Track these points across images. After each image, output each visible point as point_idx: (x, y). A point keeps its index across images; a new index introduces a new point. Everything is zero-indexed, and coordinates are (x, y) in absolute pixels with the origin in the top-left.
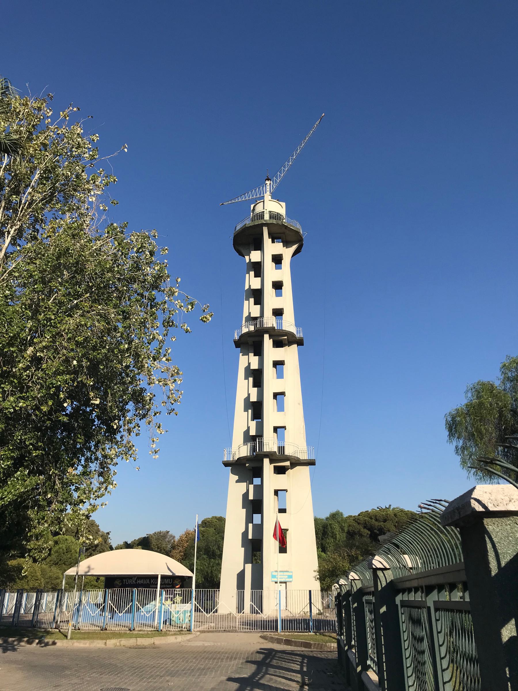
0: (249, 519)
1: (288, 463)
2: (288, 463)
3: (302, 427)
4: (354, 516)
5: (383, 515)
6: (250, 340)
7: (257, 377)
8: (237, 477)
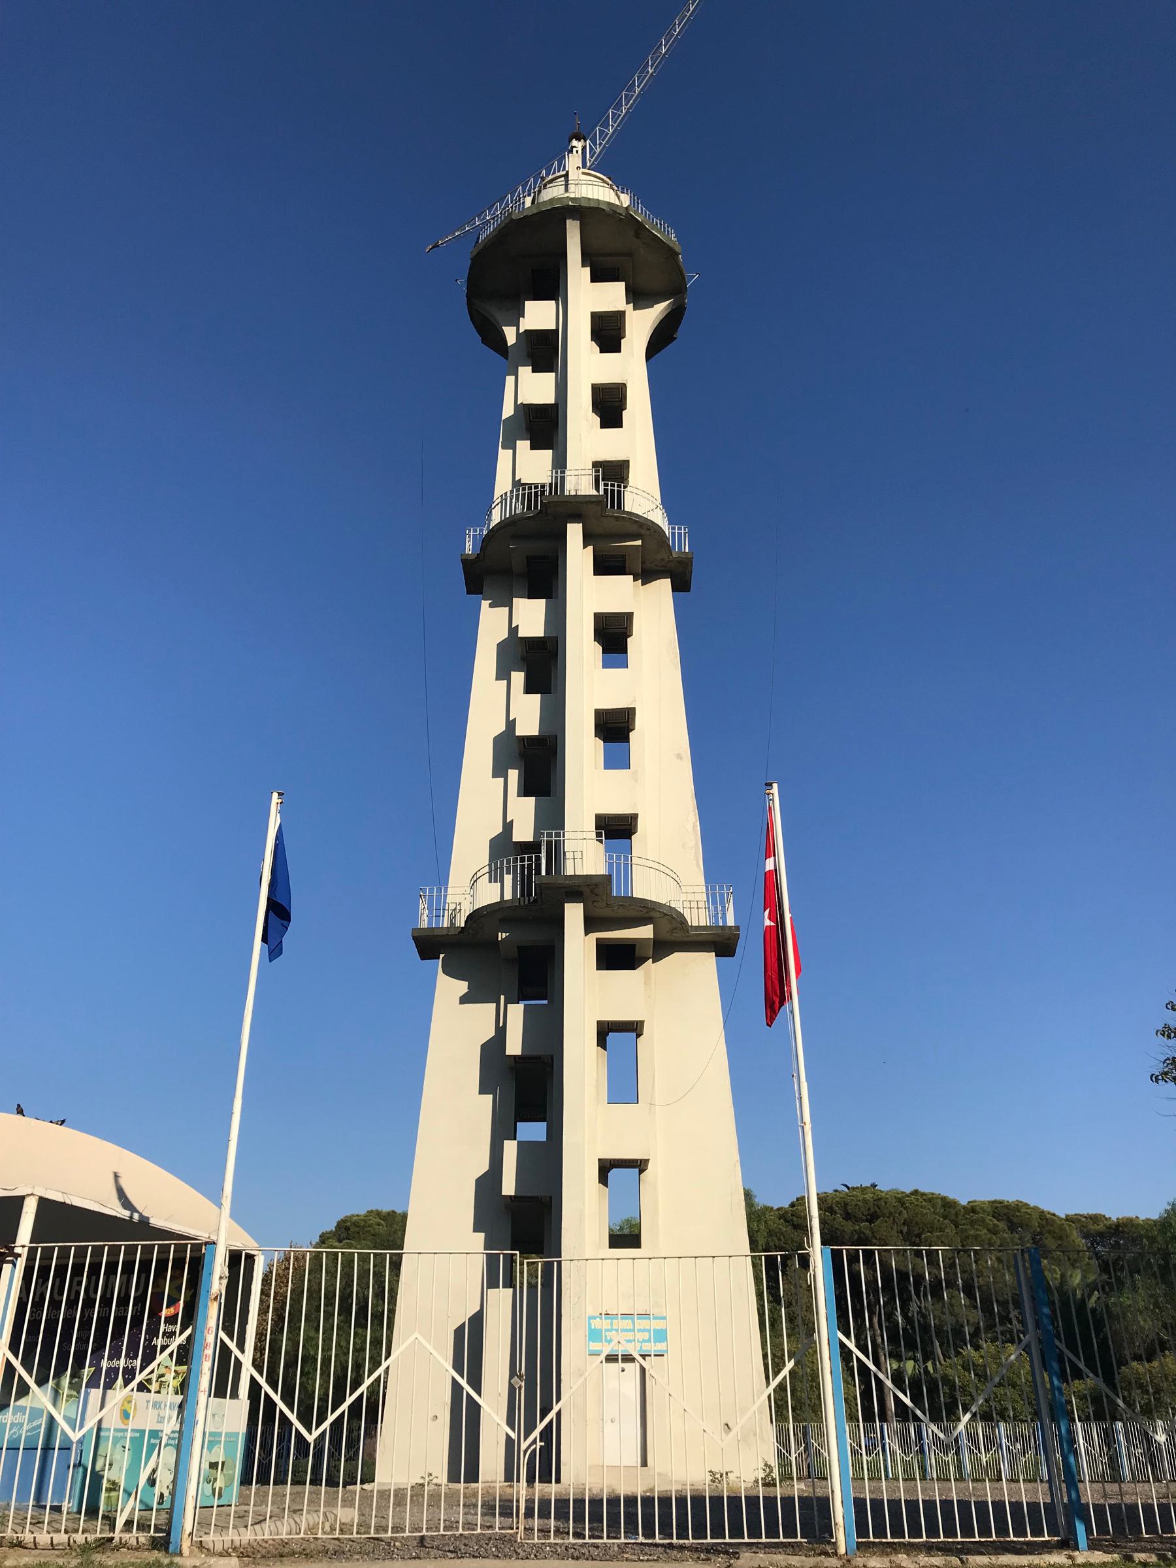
0: (501, 1131)
2: (645, 932)
3: (690, 826)
4: (778, 1209)
5: (865, 1201)
7: (539, 663)
8: (462, 987)
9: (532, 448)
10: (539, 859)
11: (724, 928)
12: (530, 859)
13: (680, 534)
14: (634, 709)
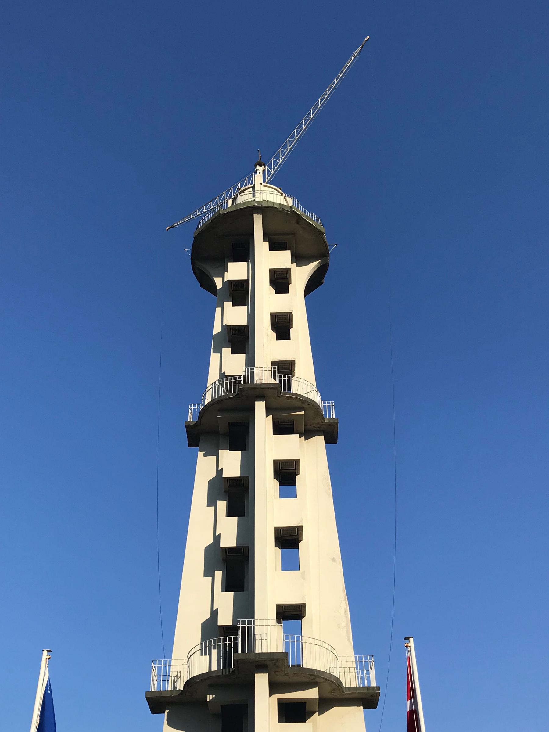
1: (313, 693)
2: (313, 693)
3: (342, 611)
6: (222, 420)
7: (237, 495)
9: (233, 306)
10: (236, 639)
11: (368, 688)
12: (230, 639)
13: (329, 406)
14: (302, 526)
